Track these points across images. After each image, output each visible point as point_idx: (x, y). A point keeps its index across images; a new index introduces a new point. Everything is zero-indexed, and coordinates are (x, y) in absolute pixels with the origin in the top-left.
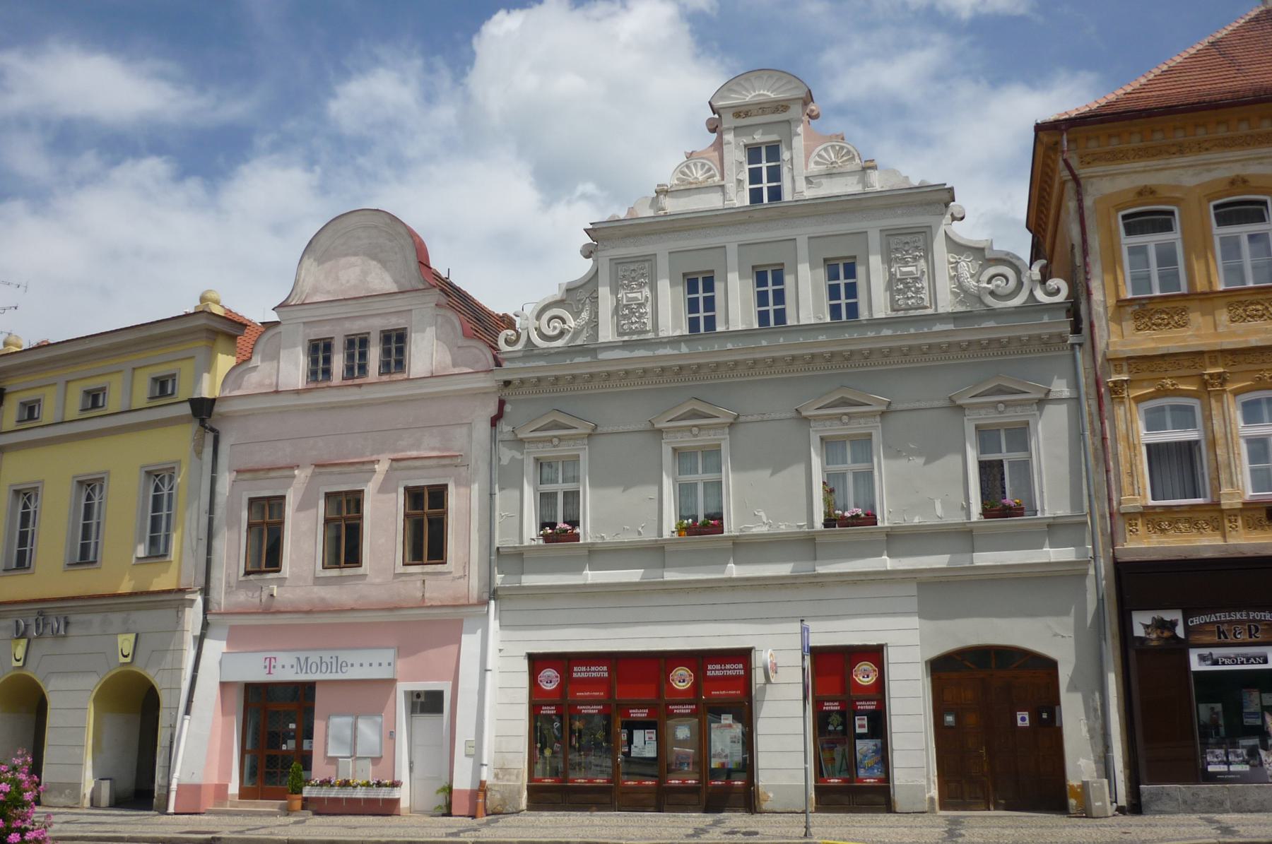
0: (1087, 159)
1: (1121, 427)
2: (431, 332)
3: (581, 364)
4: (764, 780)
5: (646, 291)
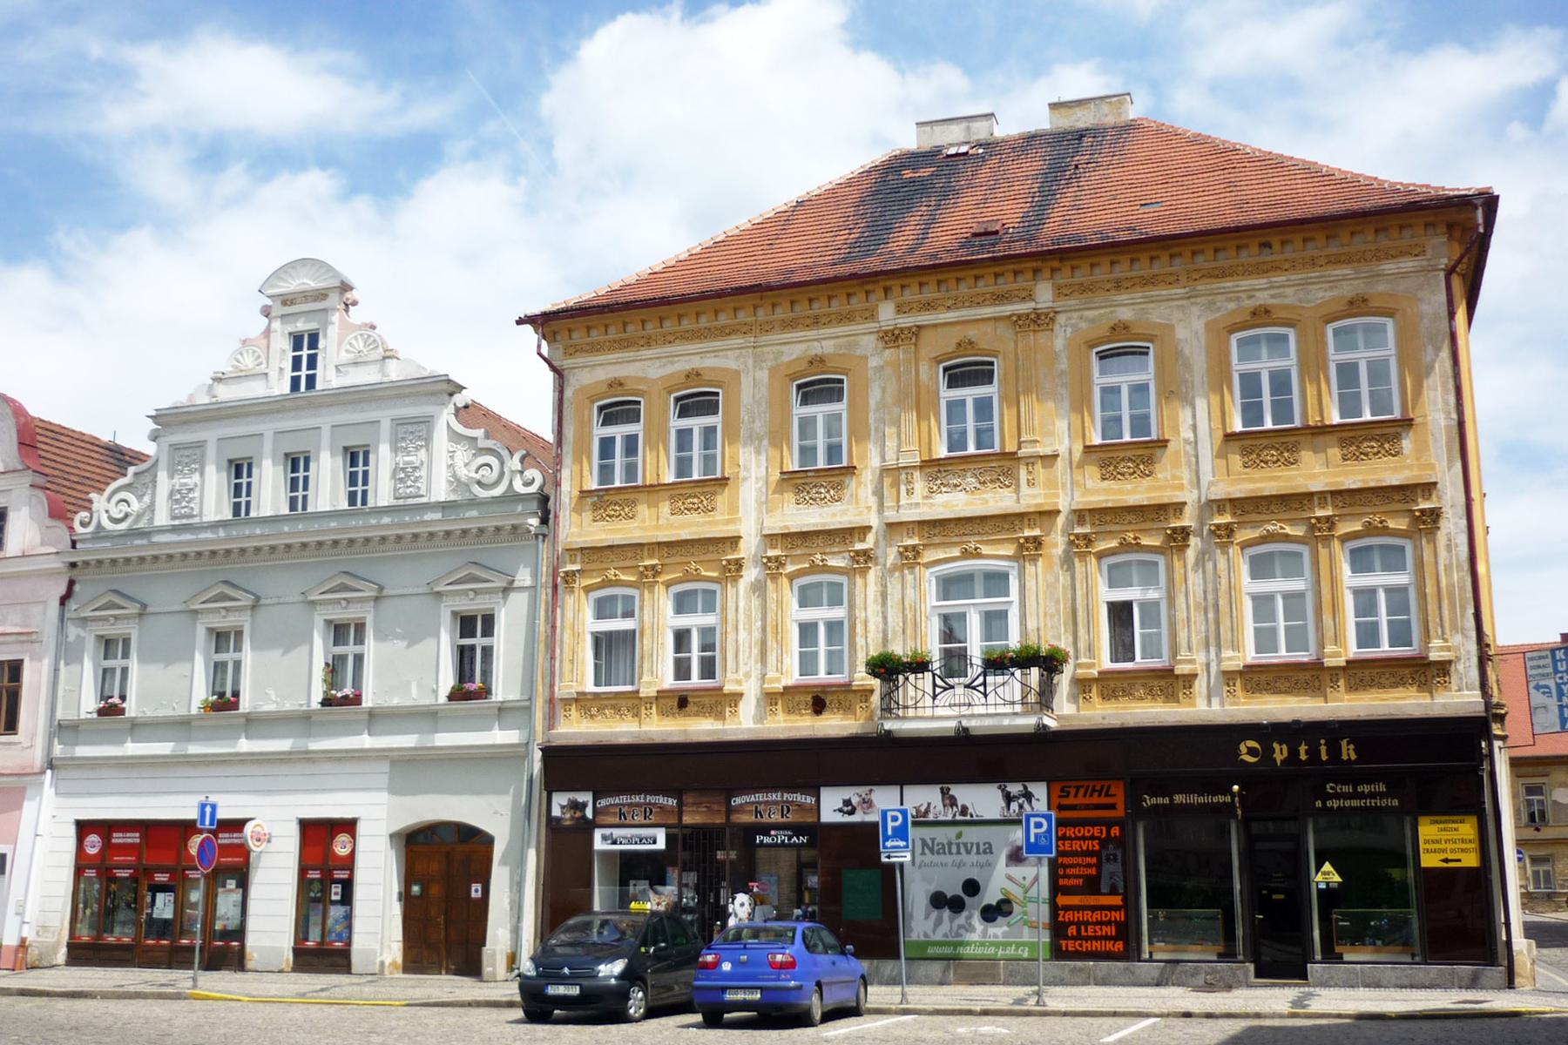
0: (571, 350)
1: (569, 614)
2: (25, 511)
3: (138, 548)
4: (252, 941)
5: (196, 477)
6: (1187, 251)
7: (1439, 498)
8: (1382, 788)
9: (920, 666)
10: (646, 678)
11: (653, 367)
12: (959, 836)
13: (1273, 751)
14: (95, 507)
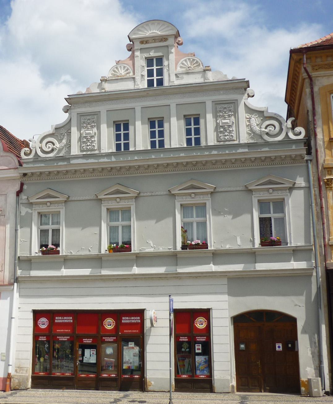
0: (316, 68)
5: (95, 130)
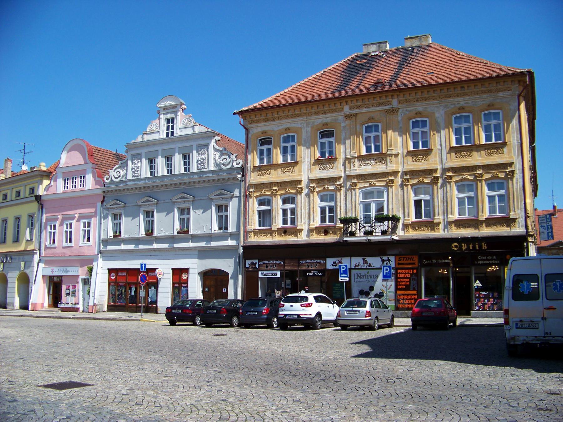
3: (123, 186)
4: (159, 305)
6: (439, 89)
7: (515, 167)
8: (495, 257)
9: (356, 220)
10: (274, 224)
11: (274, 127)
12: (368, 273)
13: (462, 246)
14: (110, 174)
